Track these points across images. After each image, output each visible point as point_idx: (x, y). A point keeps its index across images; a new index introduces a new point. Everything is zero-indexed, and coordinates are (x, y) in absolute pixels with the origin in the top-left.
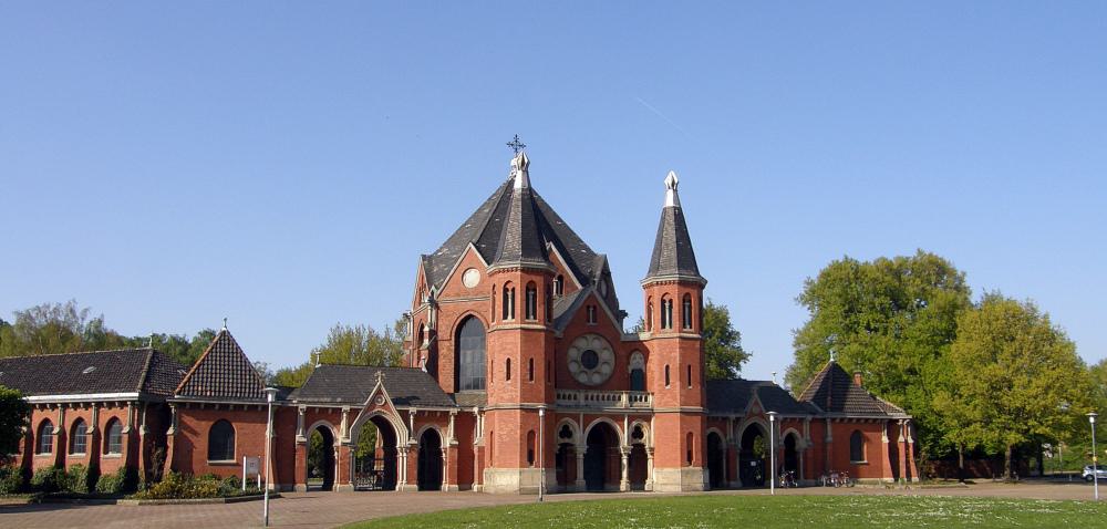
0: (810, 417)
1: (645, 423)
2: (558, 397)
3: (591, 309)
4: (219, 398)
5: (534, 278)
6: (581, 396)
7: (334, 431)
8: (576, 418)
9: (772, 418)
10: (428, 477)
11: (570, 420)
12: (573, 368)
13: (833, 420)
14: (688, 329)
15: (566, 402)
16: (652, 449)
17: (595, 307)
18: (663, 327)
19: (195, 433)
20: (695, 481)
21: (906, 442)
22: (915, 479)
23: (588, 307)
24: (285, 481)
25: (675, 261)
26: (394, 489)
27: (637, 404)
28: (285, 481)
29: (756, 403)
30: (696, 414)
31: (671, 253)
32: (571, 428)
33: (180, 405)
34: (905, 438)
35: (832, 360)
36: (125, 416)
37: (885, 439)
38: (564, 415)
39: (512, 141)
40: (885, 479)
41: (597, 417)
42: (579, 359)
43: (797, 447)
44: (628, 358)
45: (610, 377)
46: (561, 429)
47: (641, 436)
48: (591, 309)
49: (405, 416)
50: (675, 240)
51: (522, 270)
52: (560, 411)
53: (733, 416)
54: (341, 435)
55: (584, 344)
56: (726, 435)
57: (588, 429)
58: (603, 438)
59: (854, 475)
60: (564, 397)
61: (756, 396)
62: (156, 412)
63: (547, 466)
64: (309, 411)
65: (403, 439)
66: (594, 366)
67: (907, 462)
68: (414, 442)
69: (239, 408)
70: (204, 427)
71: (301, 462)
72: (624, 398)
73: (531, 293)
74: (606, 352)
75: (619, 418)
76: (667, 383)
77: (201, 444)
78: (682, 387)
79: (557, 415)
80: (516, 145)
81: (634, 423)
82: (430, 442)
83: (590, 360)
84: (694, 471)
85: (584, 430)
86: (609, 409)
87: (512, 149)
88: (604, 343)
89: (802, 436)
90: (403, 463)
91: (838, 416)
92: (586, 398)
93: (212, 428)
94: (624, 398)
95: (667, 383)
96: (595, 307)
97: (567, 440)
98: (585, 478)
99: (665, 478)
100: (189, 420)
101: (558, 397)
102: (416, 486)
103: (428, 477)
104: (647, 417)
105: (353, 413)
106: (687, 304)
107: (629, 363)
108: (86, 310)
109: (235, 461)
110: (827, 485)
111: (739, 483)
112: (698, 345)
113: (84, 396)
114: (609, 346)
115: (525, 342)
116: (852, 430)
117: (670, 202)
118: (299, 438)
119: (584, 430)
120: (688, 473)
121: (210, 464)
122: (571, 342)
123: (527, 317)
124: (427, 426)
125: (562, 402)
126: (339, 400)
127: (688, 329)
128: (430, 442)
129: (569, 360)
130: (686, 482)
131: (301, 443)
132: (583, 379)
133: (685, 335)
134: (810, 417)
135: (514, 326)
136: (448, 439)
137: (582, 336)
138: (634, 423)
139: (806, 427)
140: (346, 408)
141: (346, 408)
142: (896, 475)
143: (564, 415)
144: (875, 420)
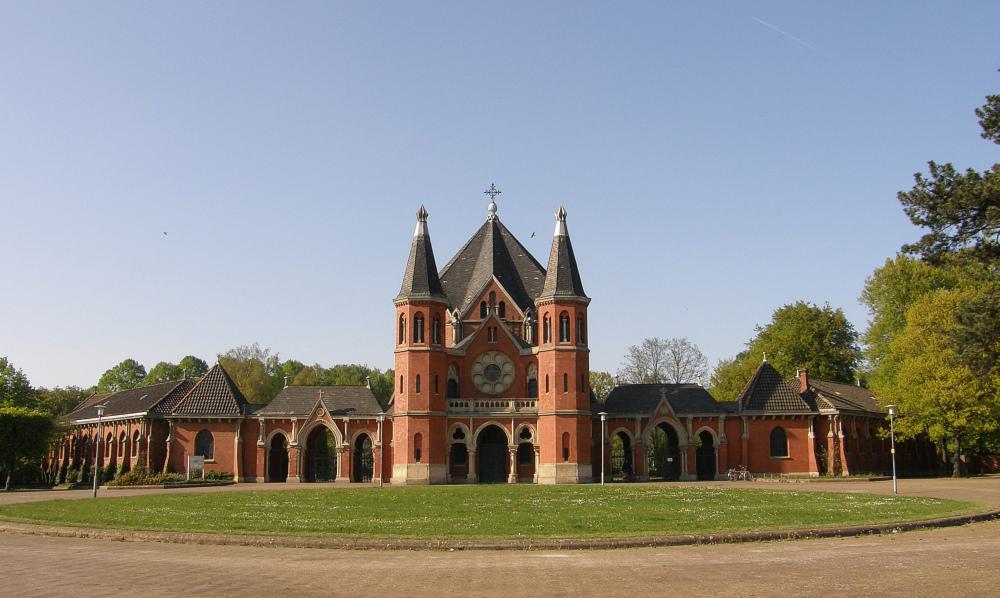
0: (723, 416)
1: (531, 425)
2: (452, 405)
3: (492, 330)
4: (202, 414)
5: (421, 309)
6: (471, 404)
7: (288, 437)
8: (466, 422)
9: (603, 418)
10: (360, 472)
11: (461, 424)
12: (478, 380)
13: (750, 418)
14: (565, 341)
15: (459, 409)
16: (538, 447)
17: (495, 328)
18: (416, 341)
19: (186, 440)
20: (569, 474)
21: (836, 437)
22: (846, 473)
23: (489, 328)
24: (248, 474)
25: (555, 284)
26: (506, 481)
27: (523, 410)
28: (248, 474)
29: (664, 404)
30: (572, 416)
31: (424, 272)
32: (463, 431)
33: (175, 420)
34: (835, 434)
35: (765, 360)
36: (139, 427)
37: (811, 435)
38: (457, 420)
39: (497, 188)
40: (811, 473)
41: (486, 420)
42: (482, 373)
43: (714, 445)
44: (527, 369)
45: (511, 387)
46: (454, 431)
47: (529, 436)
48: (492, 330)
49: (340, 424)
50: (556, 264)
51: (411, 303)
52: (451, 416)
53: (639, 417)
54: (291, 439)
55: (487, 360)
56: (717, 433)
57: (478, 431)
58: (492, 438)
59: (775, 469)
60: (457, 405)
61: (664, 398)
62: (158, 424)
63: (580, 462)
64: (267, 422)
65: (339, 442)
66: (496, 379)
67: (837, 456)
68: (347, 444)
69: (788, 417)
70: (191, 435)
71: (261, 460)
72: (512, 404)
73: (565, 320)
74: (507, 365)
75: (506, 421)
76: (547, 391)
77: (190, 447)
78: (558, 393)
79: (449, 420)
80: (493, 192)
81: (521, 425)
82: (360, 445)
83: (493, 373)
84: (569, 466)
85: (473, 434)
86: (498, 413)
87: (489, 196)
88: (493, 354)
89: (717, 433)
90: (341, 461)
91: (755, 413)
92: (477, 405)
93: (198, 436)
94: (512, 404)
95: (566, 391)
96: (495, 328)
97: (459, 441)
98: (476, 472)
99: (546, 471)
100: (181, 431)
101: (452, 405)
102: (348, 479)
103: (360, 472)
104: (534, 420)
105: (300, 422)
106: (436, 322)
107: (527, 374)
108: (267, 350)
109: (212, 460)
110: (738, 479)
111: (694, 476)
112: (574, 355)
113: (119, 416)
114: (509, 360)
115: (412, 361)
116: (772, 427)
117: (557, 232)
118: (260, 442)
119: (473, 434)
120: (562, 467)
121: (206, 463)
122: (475, 358)
123: (416, 341)
124: (359, 432)
125: (454, 409)
126: (292, 413)
127: (565, 341)
128: (360, 445)
129: (473, 373)
130: (562, 475)
131: (261, 446)
132: (487, 389)
133: (560, 347)
134: (723, 416)
135: (426, 348)
136: (376, 439)
137: (485, 353)
138: (521, 425)
139: (721, 426)
140: (294, 419)
141: (294, 419)
142: (822, 469)
143: (457, 420)
144: (798, 417)
